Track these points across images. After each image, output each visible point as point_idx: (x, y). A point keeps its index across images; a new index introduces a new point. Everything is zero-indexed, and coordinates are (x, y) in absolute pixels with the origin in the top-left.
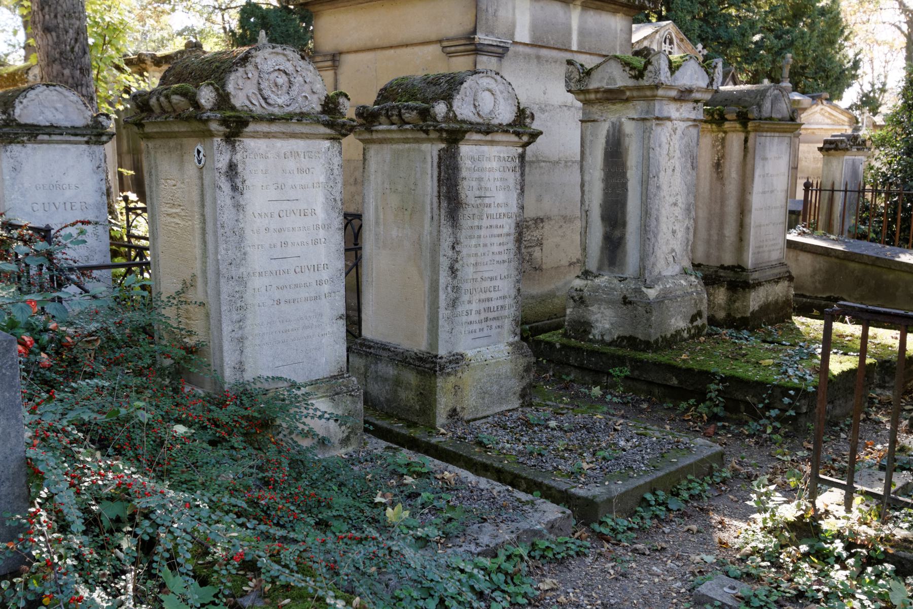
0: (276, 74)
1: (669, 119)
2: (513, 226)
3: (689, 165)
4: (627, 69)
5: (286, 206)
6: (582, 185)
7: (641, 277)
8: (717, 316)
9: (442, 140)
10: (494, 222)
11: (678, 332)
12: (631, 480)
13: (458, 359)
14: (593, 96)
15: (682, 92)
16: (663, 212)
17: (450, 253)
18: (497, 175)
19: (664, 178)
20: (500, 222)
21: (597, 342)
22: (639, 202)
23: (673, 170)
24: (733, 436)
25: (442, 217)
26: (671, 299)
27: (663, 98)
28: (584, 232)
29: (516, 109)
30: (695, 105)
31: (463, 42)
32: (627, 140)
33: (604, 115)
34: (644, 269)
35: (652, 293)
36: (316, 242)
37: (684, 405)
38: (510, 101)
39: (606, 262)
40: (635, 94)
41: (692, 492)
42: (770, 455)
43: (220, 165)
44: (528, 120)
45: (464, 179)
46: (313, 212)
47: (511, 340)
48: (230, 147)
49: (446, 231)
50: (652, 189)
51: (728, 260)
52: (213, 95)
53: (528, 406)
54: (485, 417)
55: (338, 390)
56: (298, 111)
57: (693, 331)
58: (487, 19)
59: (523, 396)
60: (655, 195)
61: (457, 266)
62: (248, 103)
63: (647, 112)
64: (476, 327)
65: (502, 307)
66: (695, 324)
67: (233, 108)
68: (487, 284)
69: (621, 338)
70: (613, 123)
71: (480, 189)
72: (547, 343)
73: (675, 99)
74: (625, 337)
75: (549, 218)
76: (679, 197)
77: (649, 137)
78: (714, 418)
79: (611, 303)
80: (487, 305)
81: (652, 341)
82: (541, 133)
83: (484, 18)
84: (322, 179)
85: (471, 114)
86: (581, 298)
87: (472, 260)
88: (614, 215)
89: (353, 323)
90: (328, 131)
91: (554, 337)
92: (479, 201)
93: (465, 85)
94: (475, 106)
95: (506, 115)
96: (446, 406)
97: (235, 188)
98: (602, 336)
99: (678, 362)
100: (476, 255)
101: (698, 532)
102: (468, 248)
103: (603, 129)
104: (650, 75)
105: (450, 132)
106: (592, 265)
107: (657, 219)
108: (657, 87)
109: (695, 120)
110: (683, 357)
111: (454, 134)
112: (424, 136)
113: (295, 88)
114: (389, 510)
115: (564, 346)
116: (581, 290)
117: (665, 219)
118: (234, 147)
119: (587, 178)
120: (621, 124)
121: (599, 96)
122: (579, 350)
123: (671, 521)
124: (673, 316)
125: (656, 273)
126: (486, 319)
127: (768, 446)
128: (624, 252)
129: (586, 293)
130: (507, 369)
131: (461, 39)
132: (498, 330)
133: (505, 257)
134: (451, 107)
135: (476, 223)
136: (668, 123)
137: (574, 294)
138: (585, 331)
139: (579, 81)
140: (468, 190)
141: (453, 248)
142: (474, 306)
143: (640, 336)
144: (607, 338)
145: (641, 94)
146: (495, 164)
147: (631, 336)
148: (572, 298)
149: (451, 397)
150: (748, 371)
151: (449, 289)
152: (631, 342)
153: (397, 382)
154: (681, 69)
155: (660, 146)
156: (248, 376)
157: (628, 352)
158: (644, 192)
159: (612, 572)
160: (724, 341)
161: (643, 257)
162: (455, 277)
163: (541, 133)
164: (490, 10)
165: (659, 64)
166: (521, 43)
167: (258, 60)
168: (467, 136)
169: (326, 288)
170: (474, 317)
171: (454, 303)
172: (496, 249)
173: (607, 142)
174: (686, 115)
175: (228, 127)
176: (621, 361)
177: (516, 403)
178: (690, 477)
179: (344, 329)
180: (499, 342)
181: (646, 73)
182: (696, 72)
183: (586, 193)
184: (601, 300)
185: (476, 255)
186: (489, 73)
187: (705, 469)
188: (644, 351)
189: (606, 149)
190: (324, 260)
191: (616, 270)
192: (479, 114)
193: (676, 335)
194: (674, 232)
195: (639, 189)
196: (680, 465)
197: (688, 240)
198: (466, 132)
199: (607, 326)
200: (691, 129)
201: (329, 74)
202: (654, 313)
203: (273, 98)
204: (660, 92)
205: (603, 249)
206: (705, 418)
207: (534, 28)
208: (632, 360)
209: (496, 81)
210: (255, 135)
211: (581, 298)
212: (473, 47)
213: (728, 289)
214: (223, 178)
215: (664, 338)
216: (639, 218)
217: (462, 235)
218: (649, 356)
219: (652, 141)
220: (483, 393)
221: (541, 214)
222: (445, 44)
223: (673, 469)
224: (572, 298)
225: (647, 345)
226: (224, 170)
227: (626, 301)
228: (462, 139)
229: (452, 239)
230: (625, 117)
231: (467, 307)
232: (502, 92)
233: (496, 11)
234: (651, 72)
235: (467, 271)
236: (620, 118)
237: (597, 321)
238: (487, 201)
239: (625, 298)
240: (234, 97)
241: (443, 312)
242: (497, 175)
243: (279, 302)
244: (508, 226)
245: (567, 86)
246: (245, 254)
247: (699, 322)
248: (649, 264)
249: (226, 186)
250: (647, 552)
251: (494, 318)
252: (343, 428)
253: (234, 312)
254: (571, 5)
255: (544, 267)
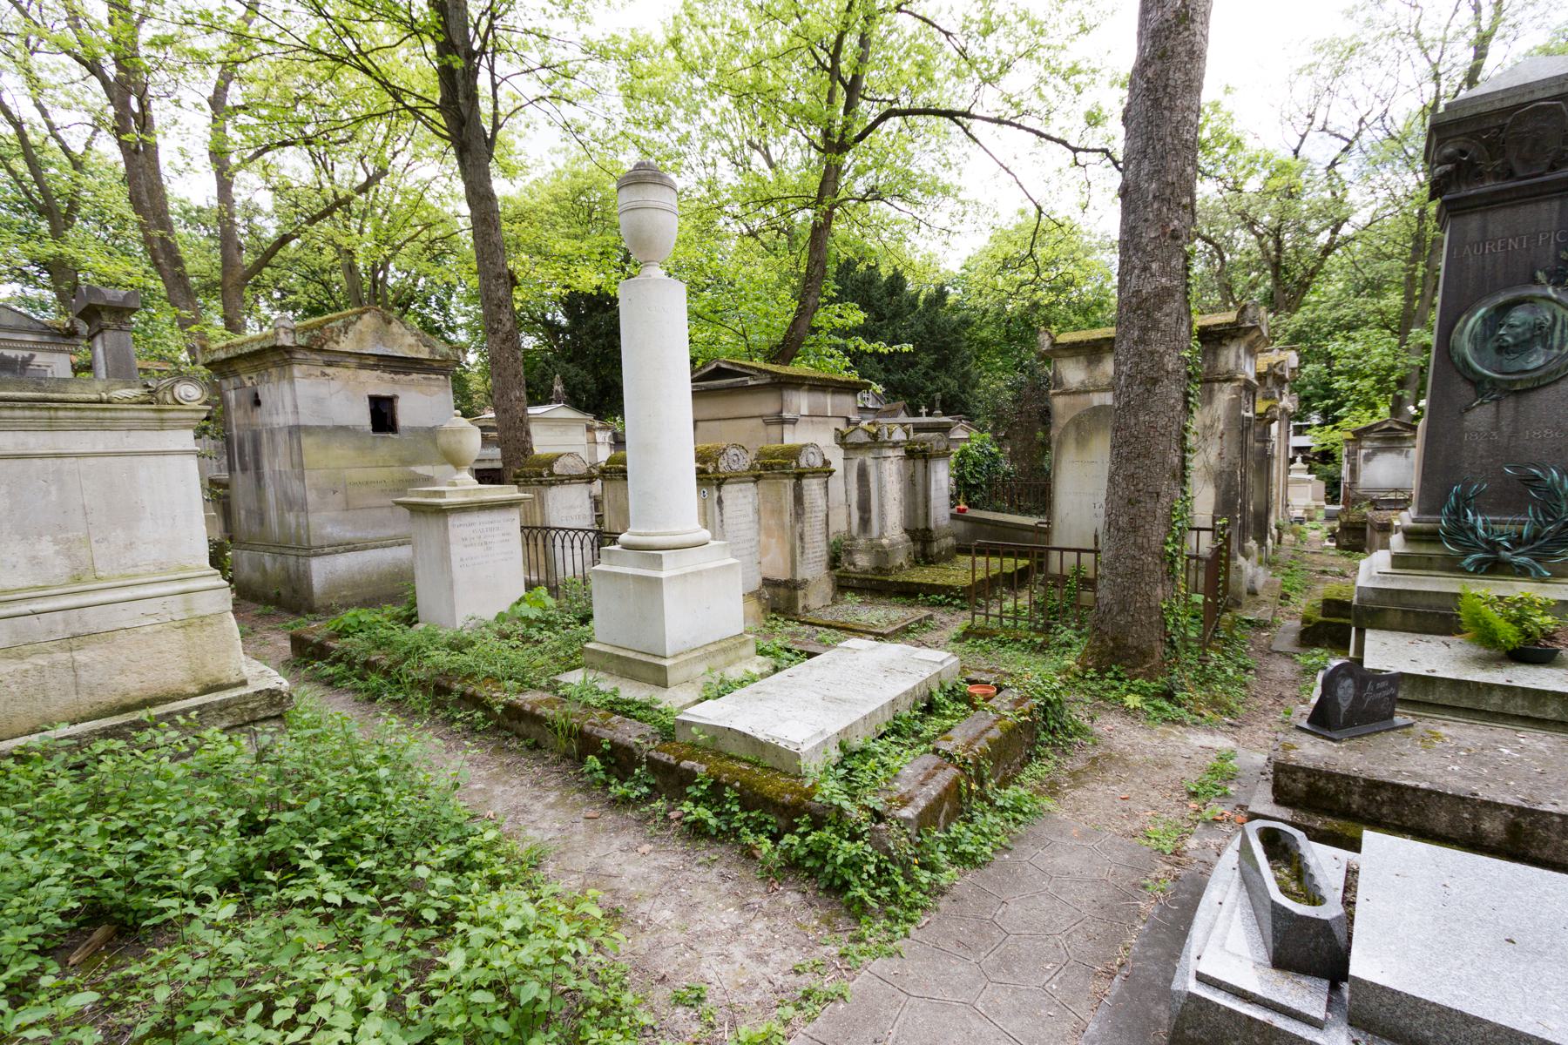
13: (805, 582)
51: (921, 526)
88: (864, 507)
89: (1514, 829)
95: (819, 463)
103: (855, 464)
111: (800, 476)
140: (807, 500)
207: (809, 407)
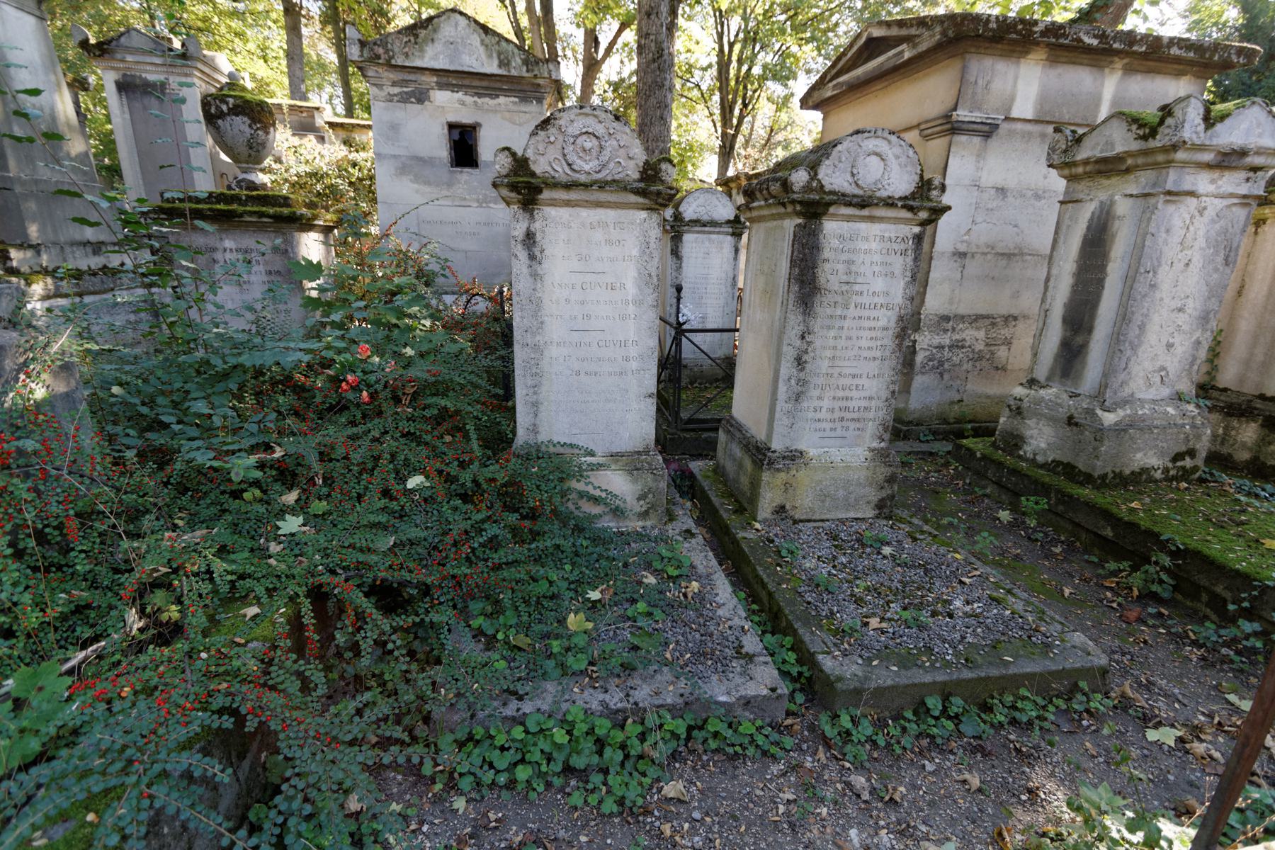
0: (585, 137)
1: (1192, 194)
2: (894, 319)
3: (1220, 259)
4: (1134, 127)
5: (589, 278)
6: (1047, 280)
7: (1099, 396)
8: (1236, 457)
9: (798, 214)
10: (866, 313)
11: (1144, 470)
12: (915, 670)
13: (794, 456)
14: (1080, 170)
15: (1225, 154)
16: (1156, 319)
17: (798, 343)
18: (877, 258)
19: (1165, 276)
20: (875, 313)
21: (1026, 460)
22: (1116, 304)
23: (1187, 264)
24: (1169, 633)
25: (791, 302)
26: (1141, 429)
27: (1185, 164)
28: (1039, 336)
29: (917, 178)
30: (1251, 174)
31: (939, 122)
32: (1117, 223)
33: (1093, 193)
34: (1106, 387)
35: (1109, 419)
36: (624, 318)
37: (1112, 566)
38: (909, 168)
39: (1058, 372)
40: (1140, 161)
41: (1017, 715)
42: (1217, 688)
43: (516, 233)
44: (935, 193)
45: (825, 260)
46: (622, 286)
47: (875, 445)
48: (527, 215)
49: (795, 319)
50: (1141, 287)
52: (509, 160)
53: (886, 518)
54: (823, 521)
55: (639, 466)
56: (609, 178)
57: (1172, 473)
58: (974, 93)
59: (880, 505)
60: (1144, 296)
61: (805, 357)
62: (549, 169)
63: (1154, 185)
64: (824, 425)
65: (865, 408)
66: (1179, 464)
67: (533, 174)
68: (848, 381)
69: (1057, 463)
70: (1101, 202)
71: (849, 273)
72: (968, 449)
73: (1209, 166)
74: (1062, 463)
75: (1025, 317)
76: (1190, 301)
77: (1150, 219)
78: (1148, 597)
79: (1053, 420)
80: (844, 404)
81: (1096, 475)
82: (949, 208)
83: (970, 92)
84: (635, 252)
85: (846, 184)
86: (1018, 408)
87: (829, 353)
88: (1079, 319)
90: (640, 200)
91: (978, 446)
92: (845, 287)
93: (839, 147)
94: (853, 175)
96: (773, 501)
97: (532, 257)
98: (1035, 455)
99: (1123, 512)
100: (835, 348)
101: (980, 790)
102: (823, 340)
103: (1087, 211)
104: (1167, 131)
105: (806, 204)
106: (1041, 373)
107: (1142, 327)
108: (1174, 147)
109: (1245, 197)
110: (1133, 505)
112: (782, 210)
113: (606, 154)
114: (572, 615)
115: (984, 457)
116: (1020, 400)
117: (1157, 328)
118: (532, 215)
119: (1054, 271)
120: (1112, 203)
121: (1088, 168)
122: (1000, 465)
123: (951, 752)
124: (1139, 450)
125: (1126, 392)
126: (842, 419)
127: (1222, 670)
128: (1084, 364)
129: (1025, 404)
130: (862, 475)
131: (935, 119)
132: (857, 433)
133: (878, 354)
134: (816, 174)
135: (839, 312)
136: (1192, 202)
137: (1012, 403)
138: (1016, 445)
139: (1065, 151)
140: (830, 272)
141: (803, 337)
142: (826, 403)
143: (1081, 466)
144: (1040, 459)
145: (1150, 160)
146: (874, 245)
147: (1068, 464)
148: (1009, 406)
149: (780, 493)
150: (1232, 550)
151: (793, 382)
152: (1069, 470)
153: (740, 466)
154: (1227, 122)
155: (1168, 231)
156: (542, 438)
157: (1060, 482)
158: (1127, 290)
159: (782, 809)
160: (1223, 493)
161: (1107, 374)
162: (802, 369)
163: (949, 208)
164: (980, 82)
165: (1185, 114)
166: (1019, 120)
167: (562, 122)
168: (832, 210)
169: (634, 365)
170: (823, 414)
171: (798, 397)
172: (864, 343)
173: (1088, 228)
174: (1230, 189)
175: (519, 193)
176: (1043, 489)
177: (870, 513)
178: (1023, 692)
179: (654, 408)
180: (857, 445)
181: (1161, 129)
182: (1259, 125)
183: (1050, 289)
184: (1041, 415)
185: (835, 348)
186: (879, 133)
187: (1067, 687)
188: (1082, 484)
189: (1085, 236)
190: (632, 336)
191: (1069, 383)
192: (857, 184)
193: (1140, 474)
194: (1170, 346)
195: (1120, 286)
196: (1012, 670)
197: (1194, 358)
198: (830, 204)
199: (1043, 445)
200: (1234, 209)
201: (707, 155)
202: (1106, 442)
203: (579, 164)
204: (1180, 155)
205: (1058, 357)
206: (1136, 593)
208: (1058, 491)
209: (889, 142)
210: (553, 203)
211: (1018, 408)
212: (949, 126)
213: (1262, 426)
214: (519, 247)
215: (1118, 476)
216: (1112, 324)
217: (817, 325)
218: (1086, 493)
219: (1153, 224)
220: (824, 496)
221: (1015, 312)
222: (923, 127)
223: (994, 672)
224: (1009, 406)
225: (1088, 479)
226: (521, 238)
227: (1071, 421)
228: (825, 213)
229: (801, 327)
230: (1119, 196)
231: (816, 403)
232: (897, 157)
233: (988, 83)
234: (1169, 127)
235: (820, 364)
236: (1112, 196)
237: (1032, 437)
238: (857, 288)
239: (1071, 418)
240: (535, 162)
241: (781, 405)
242: (877, 258)
243: (578, 373)
244: (887, 319)
245: (1048, 160)
246: (542, 323)
247: (1188, 463)
248: (1114, 383)
249: (523, 255)
250: (866, 796)
251: (853, 419)
252: (642, 502)
253: (529, 377)
254: (1107, 70)
255: (1009, 367)
